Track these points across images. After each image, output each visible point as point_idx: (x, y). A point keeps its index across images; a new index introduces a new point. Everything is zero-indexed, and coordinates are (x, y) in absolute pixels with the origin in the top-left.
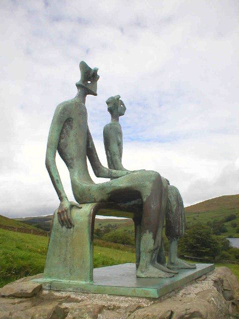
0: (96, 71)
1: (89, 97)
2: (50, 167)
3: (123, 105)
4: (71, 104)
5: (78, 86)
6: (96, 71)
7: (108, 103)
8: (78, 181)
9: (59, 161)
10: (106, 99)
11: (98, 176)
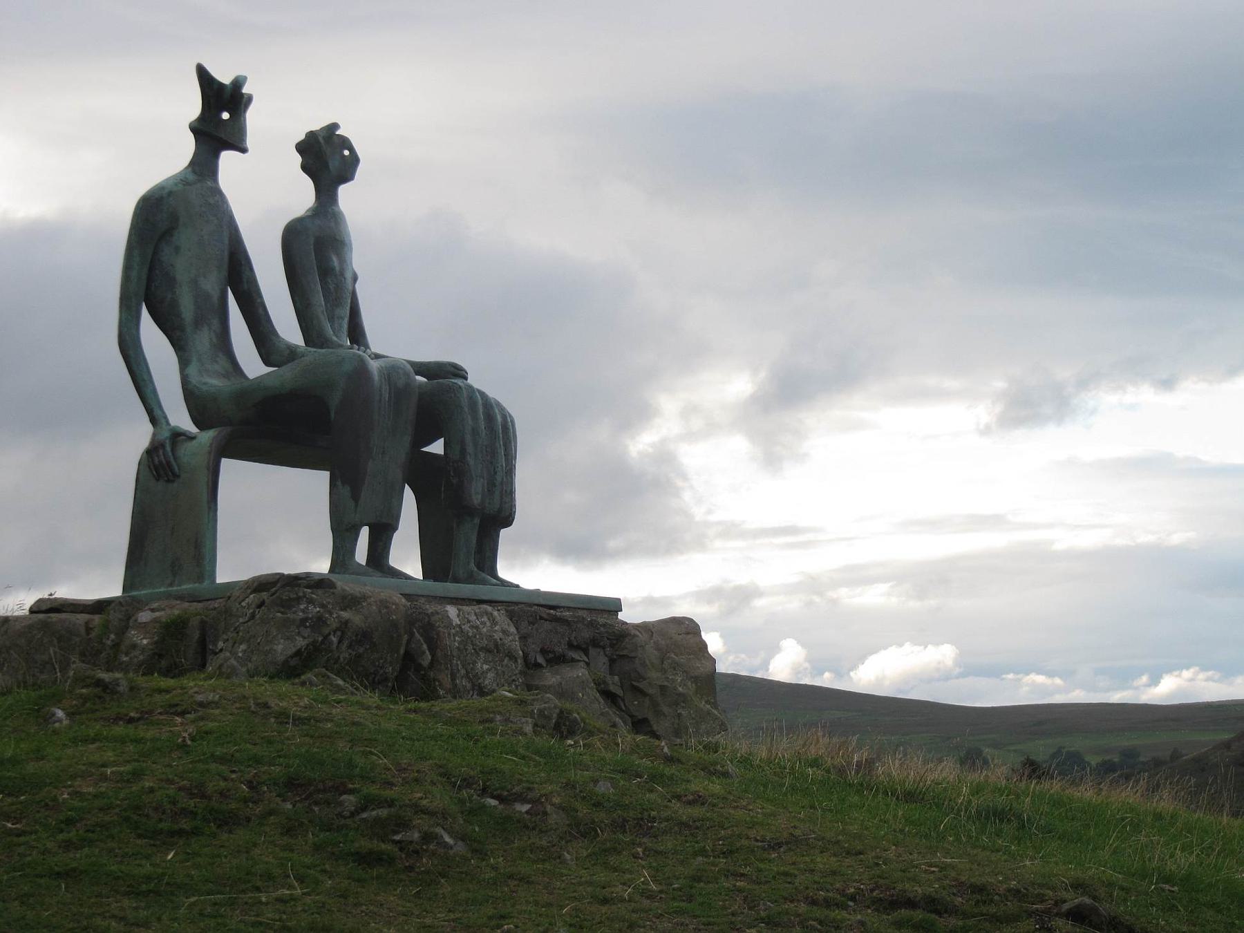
0: (238, 83)
1: (227, 159)
3: (351, 149)
9: (154, 342)
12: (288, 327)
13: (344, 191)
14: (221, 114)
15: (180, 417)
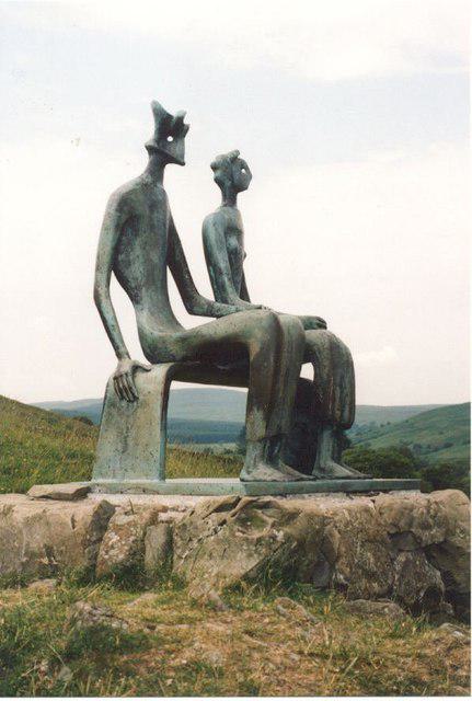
0: (180, 119)
2: (99, 300)
3: (247, 168)
4: (132, 192)
5: (150, 149)
6: (180, 119)
7: (214, 168)
8: (148, 329)
10: (213, 159)
11: (191, 311)
12: (204, 289)
13: (240, 196)
14: (169, 133)
15: (137, 355)
